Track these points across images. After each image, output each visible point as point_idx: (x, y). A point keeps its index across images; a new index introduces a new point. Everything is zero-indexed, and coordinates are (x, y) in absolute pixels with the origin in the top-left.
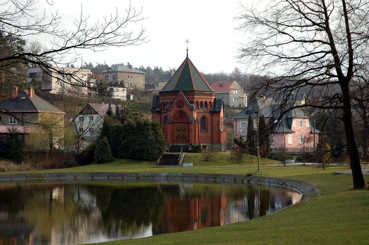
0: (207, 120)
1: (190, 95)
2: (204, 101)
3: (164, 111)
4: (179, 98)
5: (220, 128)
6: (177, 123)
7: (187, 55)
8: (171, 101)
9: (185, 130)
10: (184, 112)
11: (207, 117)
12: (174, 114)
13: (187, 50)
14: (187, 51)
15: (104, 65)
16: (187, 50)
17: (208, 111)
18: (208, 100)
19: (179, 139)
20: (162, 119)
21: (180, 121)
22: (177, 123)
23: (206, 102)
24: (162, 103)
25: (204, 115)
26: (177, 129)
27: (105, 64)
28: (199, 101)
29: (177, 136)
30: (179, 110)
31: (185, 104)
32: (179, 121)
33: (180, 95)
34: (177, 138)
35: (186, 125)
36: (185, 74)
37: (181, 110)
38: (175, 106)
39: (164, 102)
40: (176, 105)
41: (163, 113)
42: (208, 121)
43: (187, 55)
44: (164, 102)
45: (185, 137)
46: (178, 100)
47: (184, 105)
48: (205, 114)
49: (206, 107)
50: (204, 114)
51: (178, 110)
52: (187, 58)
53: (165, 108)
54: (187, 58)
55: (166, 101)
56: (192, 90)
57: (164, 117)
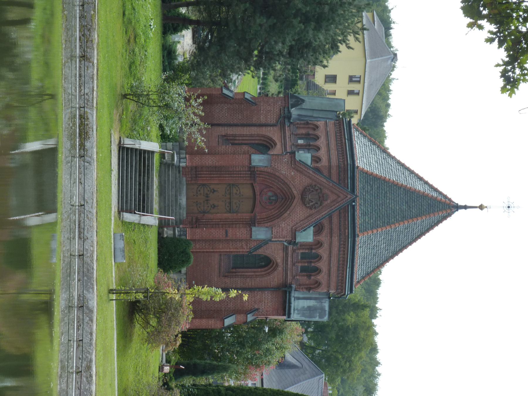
0: (262, 276)
1: (340, 221)
2: (322, 265)
3: (288, 134)
4: (332, 192)
5: (234, 316)
6: (252, 184)
7: (465, 207)
8: (320, 160)
9: (230, 212)
10: (286, 211)
11: (269, 274)
12: (282, 177)
13: (481, 207)
14: (478, 205)
15: (391, 77)
16: (481, 207)
17: (289, 277)
18: (326, 277)
19: (202, 191)
20: (264, 128)
21: (258, 197)
22: (252, 184)
23: (318, 271)
24: (314, 130)
25: (277, 265)
26: (233, 185)
27: (394, 79)
28: (323, 252)
29: (212, 187)
30: (295, 192)
31: (314, 211)
32: (258, 193)
33: (342, 196)
34: (204, 185)
35: (247, 216)
36: (407, 203)
37: (294, 198)
38: (306, 181)
39: (317, 138)
40: (311, 185)
41: (285, 133)
42: (258, 279)
43: (465, 207)
44: (318, 138)
45: (208, 212)
46: (326, 191)
47: (311, 209)
48: (280, 269)
49: (302, 258)
50: (280, 264)
51: (293, 190)
52: (458, 207)
53: (300, 139)
54: (458, 207)
55: (322, 142)
56: (357, 230)
57: (270, 135)
